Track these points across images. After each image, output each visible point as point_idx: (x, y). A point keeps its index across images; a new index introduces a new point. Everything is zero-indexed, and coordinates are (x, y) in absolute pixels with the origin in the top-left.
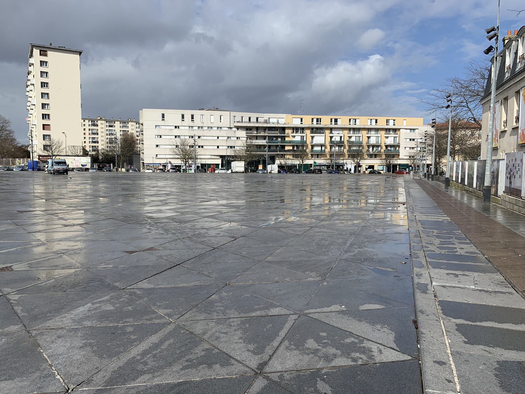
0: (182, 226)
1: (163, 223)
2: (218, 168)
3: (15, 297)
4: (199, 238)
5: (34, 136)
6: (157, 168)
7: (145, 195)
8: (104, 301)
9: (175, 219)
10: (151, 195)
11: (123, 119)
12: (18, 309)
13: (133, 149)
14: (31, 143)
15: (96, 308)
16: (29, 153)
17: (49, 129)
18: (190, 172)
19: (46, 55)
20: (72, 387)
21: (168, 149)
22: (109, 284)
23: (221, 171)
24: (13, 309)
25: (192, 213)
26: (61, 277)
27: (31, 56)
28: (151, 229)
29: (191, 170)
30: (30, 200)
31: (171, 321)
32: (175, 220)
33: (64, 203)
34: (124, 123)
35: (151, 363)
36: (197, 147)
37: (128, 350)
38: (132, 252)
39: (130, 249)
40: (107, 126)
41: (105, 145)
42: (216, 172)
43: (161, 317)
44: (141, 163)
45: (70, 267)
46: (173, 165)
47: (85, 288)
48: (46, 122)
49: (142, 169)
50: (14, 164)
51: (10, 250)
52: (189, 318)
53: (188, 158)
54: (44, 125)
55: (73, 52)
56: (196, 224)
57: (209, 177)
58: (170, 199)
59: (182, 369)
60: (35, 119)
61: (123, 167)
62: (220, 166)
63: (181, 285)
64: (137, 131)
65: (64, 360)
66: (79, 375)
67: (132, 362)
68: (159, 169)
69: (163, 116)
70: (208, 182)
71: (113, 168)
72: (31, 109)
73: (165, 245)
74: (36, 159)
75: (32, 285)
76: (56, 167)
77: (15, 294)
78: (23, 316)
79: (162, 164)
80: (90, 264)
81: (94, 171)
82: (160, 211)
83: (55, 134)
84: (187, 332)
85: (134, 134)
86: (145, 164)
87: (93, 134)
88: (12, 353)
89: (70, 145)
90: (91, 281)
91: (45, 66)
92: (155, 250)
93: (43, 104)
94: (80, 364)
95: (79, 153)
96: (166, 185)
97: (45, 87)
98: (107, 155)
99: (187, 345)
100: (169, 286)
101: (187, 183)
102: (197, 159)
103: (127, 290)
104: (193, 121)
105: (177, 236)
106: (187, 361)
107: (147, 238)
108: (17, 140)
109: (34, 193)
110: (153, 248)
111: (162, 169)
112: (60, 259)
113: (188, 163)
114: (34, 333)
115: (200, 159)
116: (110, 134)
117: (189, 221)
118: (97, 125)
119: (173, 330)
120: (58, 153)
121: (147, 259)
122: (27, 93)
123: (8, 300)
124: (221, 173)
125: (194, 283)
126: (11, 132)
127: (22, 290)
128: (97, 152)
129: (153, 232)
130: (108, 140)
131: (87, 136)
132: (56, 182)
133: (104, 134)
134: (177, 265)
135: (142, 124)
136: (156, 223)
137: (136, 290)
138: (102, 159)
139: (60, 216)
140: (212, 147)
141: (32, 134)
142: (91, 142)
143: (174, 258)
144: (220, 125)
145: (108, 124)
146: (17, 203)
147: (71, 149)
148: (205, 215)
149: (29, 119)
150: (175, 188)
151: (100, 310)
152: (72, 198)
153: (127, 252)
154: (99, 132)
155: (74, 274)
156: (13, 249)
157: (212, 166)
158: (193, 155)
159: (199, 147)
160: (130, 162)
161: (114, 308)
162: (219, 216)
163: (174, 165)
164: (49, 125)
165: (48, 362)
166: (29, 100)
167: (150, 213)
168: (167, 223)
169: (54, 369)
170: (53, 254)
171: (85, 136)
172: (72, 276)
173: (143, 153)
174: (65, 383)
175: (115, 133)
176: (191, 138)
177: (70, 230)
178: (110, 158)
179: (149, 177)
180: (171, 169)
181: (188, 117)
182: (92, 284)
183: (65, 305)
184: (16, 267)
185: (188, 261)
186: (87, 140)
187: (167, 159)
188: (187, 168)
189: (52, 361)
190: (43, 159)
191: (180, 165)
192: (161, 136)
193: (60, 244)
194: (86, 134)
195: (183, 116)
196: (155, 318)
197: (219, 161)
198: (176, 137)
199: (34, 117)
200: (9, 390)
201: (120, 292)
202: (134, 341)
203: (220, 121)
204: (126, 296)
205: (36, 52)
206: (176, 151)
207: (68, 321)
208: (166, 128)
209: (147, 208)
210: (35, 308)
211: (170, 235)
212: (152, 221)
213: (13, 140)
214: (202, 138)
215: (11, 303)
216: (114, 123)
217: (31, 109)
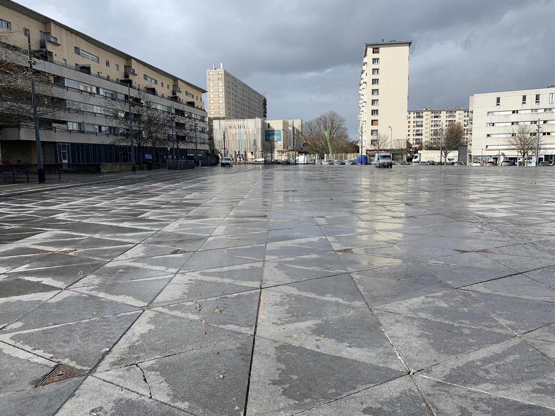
0: (523, 229)
1: (497, 223)
5: (364, 132)
6: (487, 161)
8: (437, 297)
9: (512, 220)
10: (481, 192)
12: (361, 288)
14: (360, 138)
15: (430, 302)
16: (358, 148)
17: (377, 125)
18: (529, 165)
19: (378, 52)
20: (413, 371)
22: (441, 281)
24: (356, 287)
25: (535, 215)
26: (394, 266)
27: (365, 55)
28: (483, 229)
30: (360, 191)
31: (516, 335)
32: (512, 222)
33: (391, 195)
34: (451, 112)
35: (494, 374)
36: (542, 134)
37: (466, 352)
38: (463, 252)
43: (502, 327)
46: (507, 158)
48: (374, 117)
49: (468, 162)
50: (346, 158)
52: (539, 337)
53: (528, 149)
54: (372, 121)
55: (404, 44)
58: (504, 197)
59: (533, 391)
64: (465, 121)
65: (403, 343)
66: (418, 362)
67: (471, 365)
68: (489, 163)
69: (498, 100)
73: (502, 249)
74: (364, 154)
75: (370, 268)
76: (381, 161)
79: (492, 157)
82: (493, 210)
83: (381, 128)
84: (537, 352)
85: (462, 123)
86: (472, 157)
87: (418, 126)
88: (359, 325)
89: (395, 139)
91: (377, 63)
94: (419, 352)
95: (403, 146)
97: (375, 83)
99: (537, 366)
100: (511, 295)
102: (540, 149)
106: (539, 384)
111: (493, 162)
114: (375, 312)
116: (435, 125)
118: (422, 117)
119: (518, 345)
121: (481, 261)
122: (360, 92)
123: (352, 278)
126: (345, 129)
128: (420, 145)
129: (486, 233)
132: (381, 175)
133: (428, 126)
134: (519, 273)
135: (472, 112)
136: (489, 223)
137: (471, 293)
139: (388, 207)
145: (433, 115)
149: (360, 116)
152: (398, 191)
153: (458, 250)
154: (424, 124)
158: (535, 145)
159: (544, 134)
163: (508, 157)
164: (377, 120)
165: (389, 341)
166: (361, 98)
167: (481, 211)
168: (503, 224)
169: (395, 350)
170: (385, 243)
173: (471, 144)
174: (406, 366)
179: (477, 171)
180: (503, 161)
181: (531, 98)
183: (400, 293)
186: (411, 133)
188: (525, 161)
189: (393, 342)
190: (371, 154)
191: (517, 156)
193: (390, 234)
194: (411, 127)
195: (524, 98)
196: (496, 327)
198: (513, 123)
200: (360, 356)
201: (453, 291)
202: (471, 345)
204: (460, 296)
205: (370, 50)
206: (512, 140)
207: (404, 309)
212: (484, 220)
213: (346, 137)
215: (354, 281)
216: (440, 113)
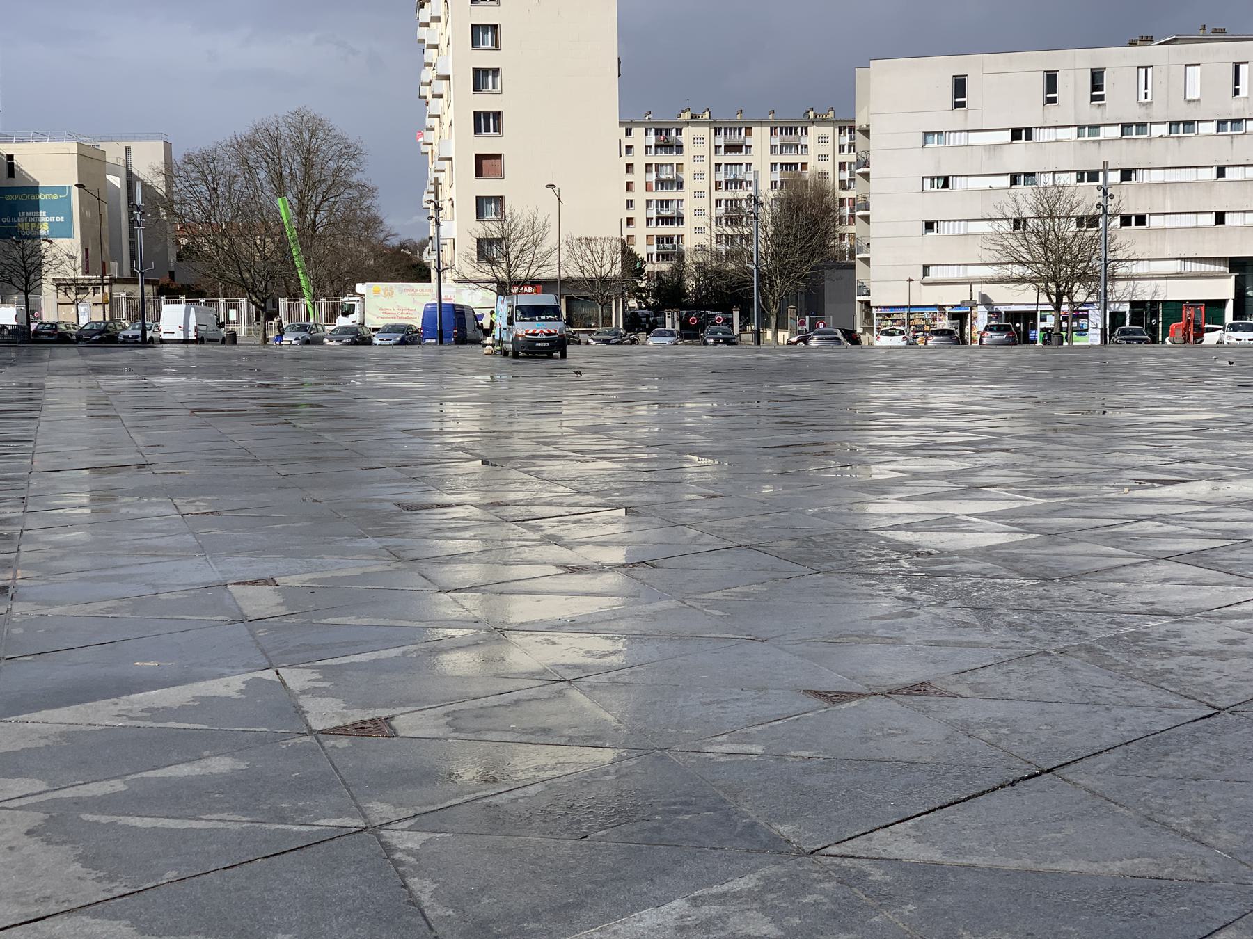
1: (964, 574)
2: (1219, 319)
3: (408, 839)
4: (1140, 654)
5: (445, 205)
6: (927, 328)
7: (881, 448)
8: (735, 895)
9: (1017, 558)
10: (906, 451)
11: (785, 116)
12: (422, 888)
13: (824, 245)
17: (500, 175)
18: (1078, 340)
21: (979, 240)
22: (753, 825)
23: (1231, 337)
24: (405, 886)
28: (912, 600)
29: (1083, 331)
32: (1019, 566)
36: (1117, 222)
38: (839, 697)
39: (832, 682)
40: (648, 147)
41: (707, 229)
42: (1210, 339)
44: (858, 305)
45: (598, 738)
46: (999, 313)
47: (659, 830)
48: (487, 144)
51: (384, 654)
54: (480, 158)
56: (1118, 591)
57: (1173, 366)
58: (990, 467)
60: (450, 137)
61: (781, 325)
62: (1229, 310)
63: (1069, 866)
68: (937, 333)
69: (960, 85)
70: (1168, 391)
71: (742, 329)
72: (435, 96)
73: (981, 677)
75: (466, 798)
77: (409, 829)
78: (443, 919)
79: (947, 309)
80: (670, 735)
81: (667, 341)
82: (951, 523)
85: (831, 175)
86: (874, 311)
87: (663, 184)
90: (683, 803)
92: (939, 693)
93: (476, 72)
95: (607, 268)
96: (971, 404)
98: (718, 273)
100: (1013, 864)
101: (1064, 395)
102: (1113, 278)
103: (829, 859)
104: (1101, 98)
105: (1035, 639)
107: (900, 641)
108: (385, 222)
109: (442, 433)
110: (928, 683)
111: (950, 333)
112: (557, 705)
113: (1071, 299)
115: (1129, 278)
116: (731, 181)
117: (1081, 576)
118: (679, 148)
120: (532, 271)
121: (906, 732)
122: (422, 33)
123: (388, 849)
124: (1230, 346)
125: (1129, 862)
126: (365, 191)
127: (430, 815)
128: (675, 262)
129: (923, 614)
130: (721, 211)
131: (640, 195)
133: (704, 186)
134: (1042, 772)
135: (866, 133)
136: (935, 574)
138: (698, 290)
139: (549, 528)
140: (1189, 221)
141: (437, 198)
142: (654, 221)
143: (1025, 738)
144: (1233, 109)
145: (721, 140)
146: (392, 472)
147: (577, 251)
148: (1161, 547)
150: (1008, 416)
151: (722, 934)
152: (588, 457)
153: (818, 694)
154: (687, 176)
155: (612, 770)
156: (394, 653)
157: (1188, 313)
159: (1126, 220)
160: (813, 304)
161: (780, 933)
162: (1233, 555)
163: (1003, 309)
167: (907, 528)
168: (984, 576)
171: (630, 196)
172: (607, 778)
173: (866, 261)
175: (750, 177)
176: (1086, 183)
177: (587, 588)
178: (729, 288)
179: (892, 366)
180: (989, 328)
181: (1074, 85)
182: (687, 817)
184: (406, 722)
185: (1091, 760)
187: (971, 283)
191: (1033, 308)
192: (946, 179)
194: (636, 186)
195: (1051, 80)
197: (1225, 289)
198: (1014, 179)
199: (446, 126)
201: (800, 864)
203: (1231, 92)
204: (827, 885)
206: (1015, 244)
208: (971, 142)
209: (884, 509)
210: (482, 890)
211: (999, 634)
212: (916, 564)
213: (373, 223)
214: (1144, 176)
215: (397, 863)
217: (435, 96)
